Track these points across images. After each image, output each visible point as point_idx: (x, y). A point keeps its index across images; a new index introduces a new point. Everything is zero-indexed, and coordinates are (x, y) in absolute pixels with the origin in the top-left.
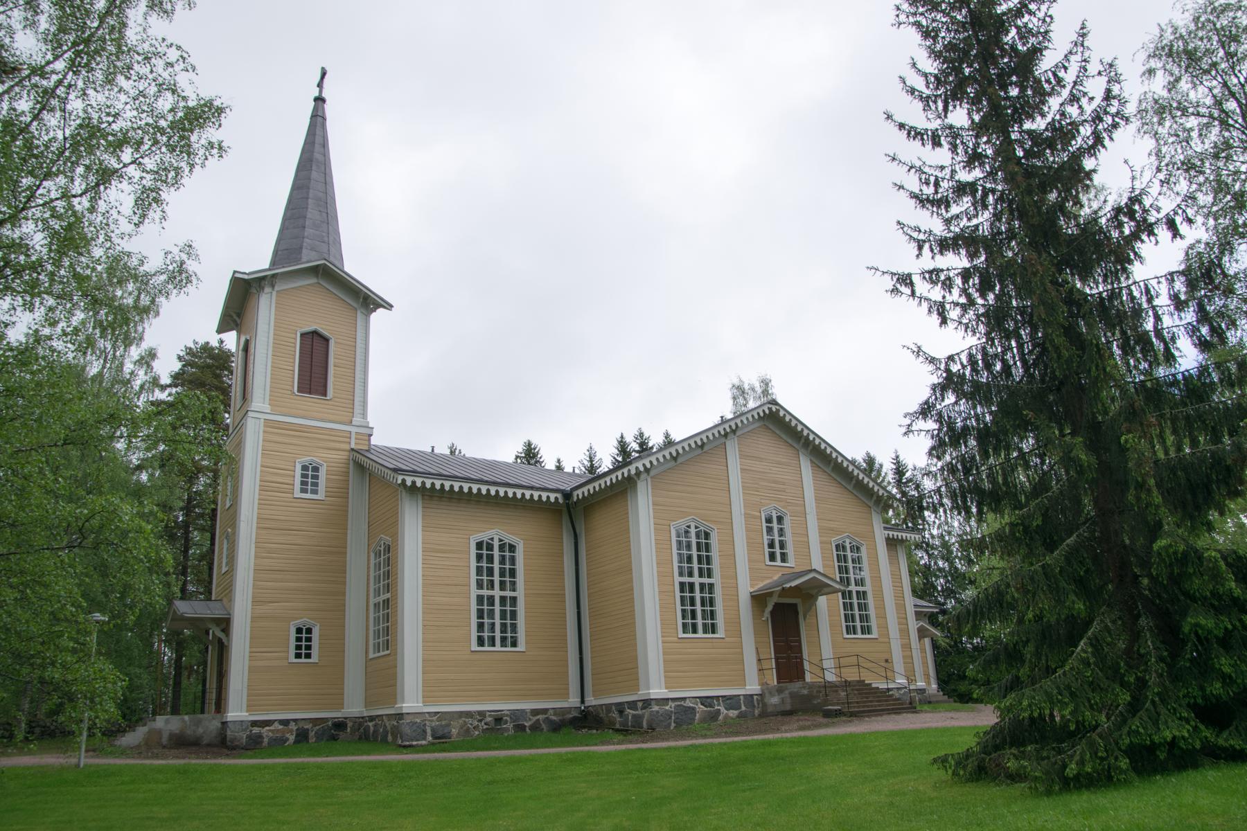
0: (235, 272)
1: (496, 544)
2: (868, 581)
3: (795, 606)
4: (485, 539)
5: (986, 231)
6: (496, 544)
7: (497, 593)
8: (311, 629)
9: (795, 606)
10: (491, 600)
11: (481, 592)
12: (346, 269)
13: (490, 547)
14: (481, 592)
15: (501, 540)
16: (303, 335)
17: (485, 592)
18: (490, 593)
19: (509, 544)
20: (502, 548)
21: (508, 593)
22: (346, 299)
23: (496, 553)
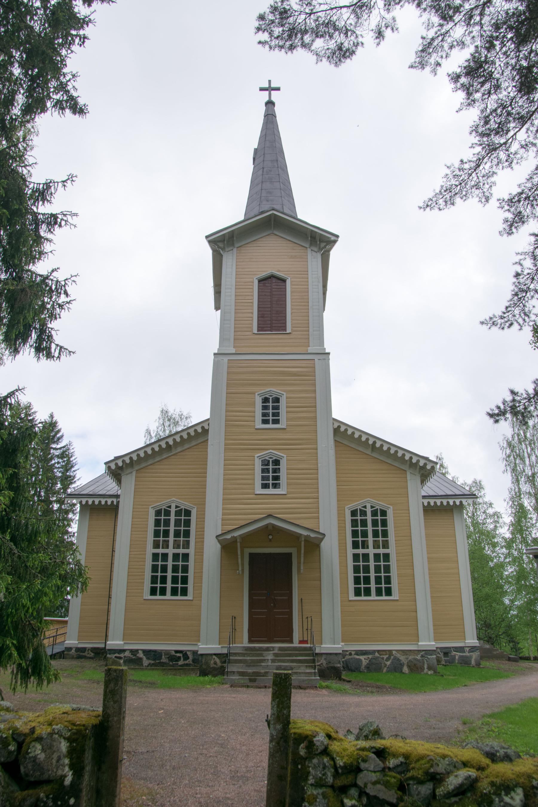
0: (207, 237)
1: (369, 511)
2: (192, 558)
3: (289, 555)
4: (359, 507)
5: (32, 682)
6: (369, 511)
7: (371, 551)
8: (190, 512)
9: (289, 555)
10: (366, 557)
11: (356, 551)
12: (300, 216)
13: (364, 513)
14: (356, 551)
15: (372, 507)
16: (260, 281)
17: (361, 551)
18: (377, 551)
19: (380, 509)
20: (374, 513)
21: (381, 551)
22: (299, 243)
23: (369, 518)
